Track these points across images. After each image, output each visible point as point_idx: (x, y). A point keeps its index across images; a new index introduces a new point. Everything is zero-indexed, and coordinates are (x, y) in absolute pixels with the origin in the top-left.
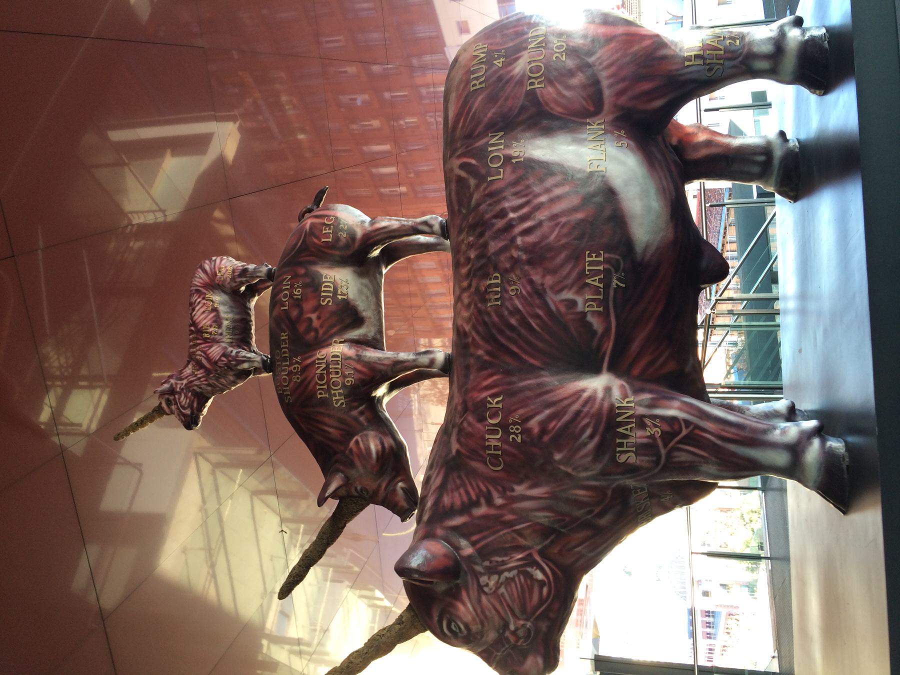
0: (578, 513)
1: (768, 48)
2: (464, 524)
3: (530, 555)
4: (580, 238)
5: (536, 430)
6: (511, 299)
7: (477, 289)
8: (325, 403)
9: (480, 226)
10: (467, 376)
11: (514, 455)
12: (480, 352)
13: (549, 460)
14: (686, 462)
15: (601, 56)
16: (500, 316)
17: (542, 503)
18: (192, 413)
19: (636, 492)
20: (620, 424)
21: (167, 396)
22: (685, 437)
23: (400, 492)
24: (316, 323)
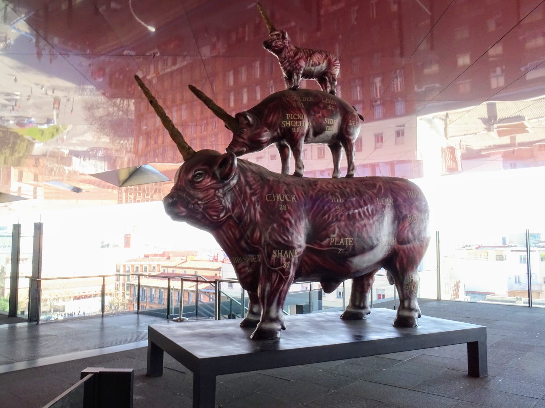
0: (248, 233)
1: (412, 306)
2: (242, 182)
3: (230, 211)
4: (358, 237)
5: (285, 216)
7: (336, 192)
10: (299, 185)
11: (274, 206)
12: (311, 192)
13: (273, 221)
14: (272, 277)
16: (327, 202)
17: (253, 218)
18: (273, 46)
19: (254, 257)
20: (288, 252)
21: (281, 35)
22: (282, 278)
23: (242, 149)
24: (318, 115)
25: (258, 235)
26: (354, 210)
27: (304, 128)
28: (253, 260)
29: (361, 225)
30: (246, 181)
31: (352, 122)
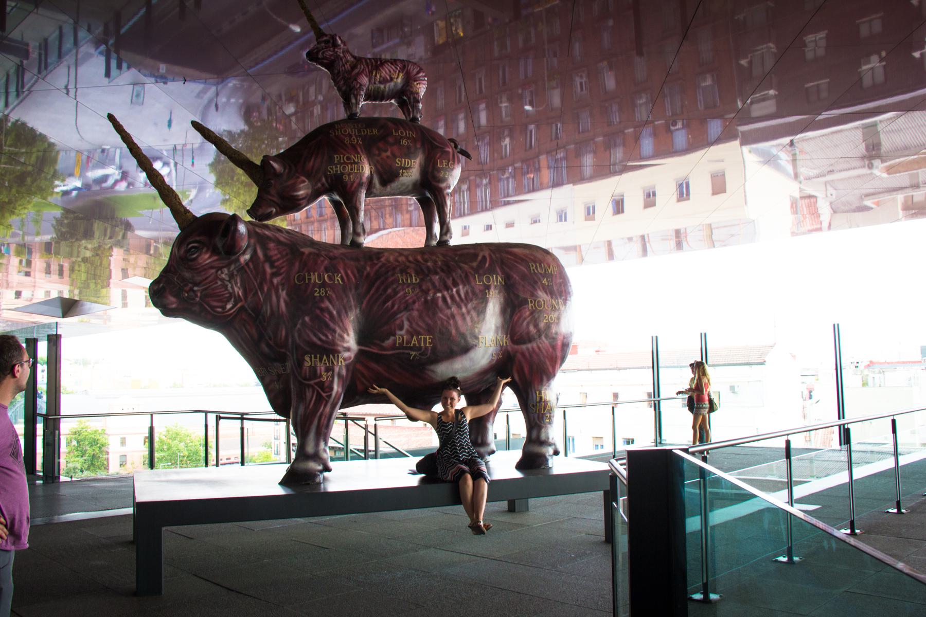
1: (543, 437)
4: (441, 332)
5: (323, 305)
6: (403, 289)
7: (408, 267)
8: (331, 161)
9: (447, 269)
12: (368, 269)
15: (544, 342)
17: (275, 309)
20: (328, 357)
22: (321, 395)
23: (269, 210)
24: (384, 155)
25: (284, 333)
26: (435, 293)
27: (361, 175)
28: (281, 371)
29: (446, 315)
30: (266, 255)
31: (442, 163)
